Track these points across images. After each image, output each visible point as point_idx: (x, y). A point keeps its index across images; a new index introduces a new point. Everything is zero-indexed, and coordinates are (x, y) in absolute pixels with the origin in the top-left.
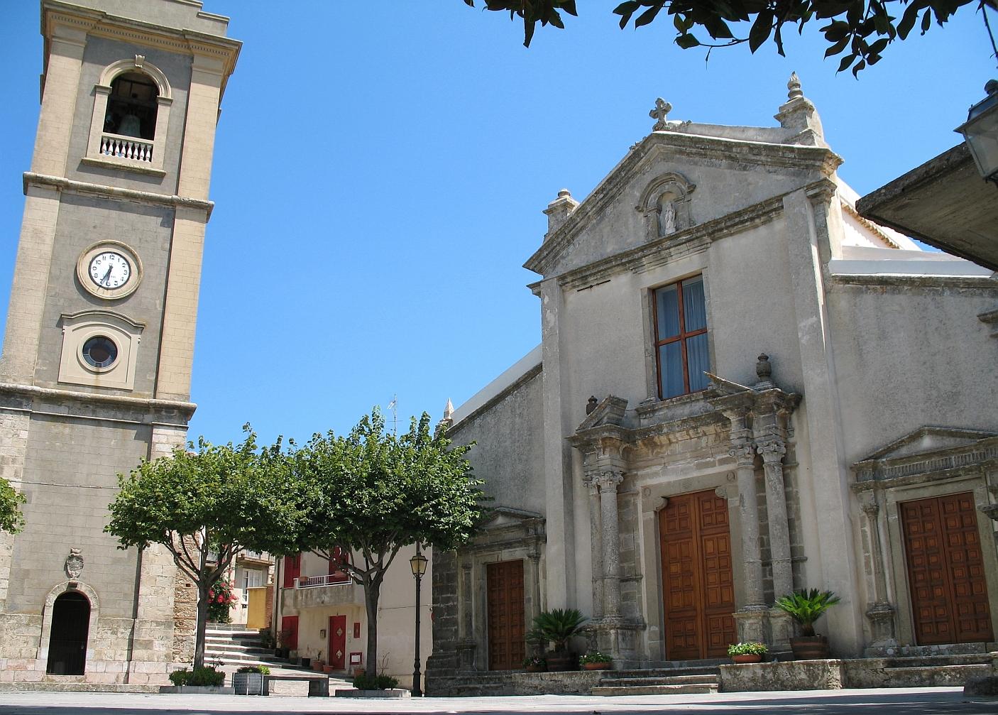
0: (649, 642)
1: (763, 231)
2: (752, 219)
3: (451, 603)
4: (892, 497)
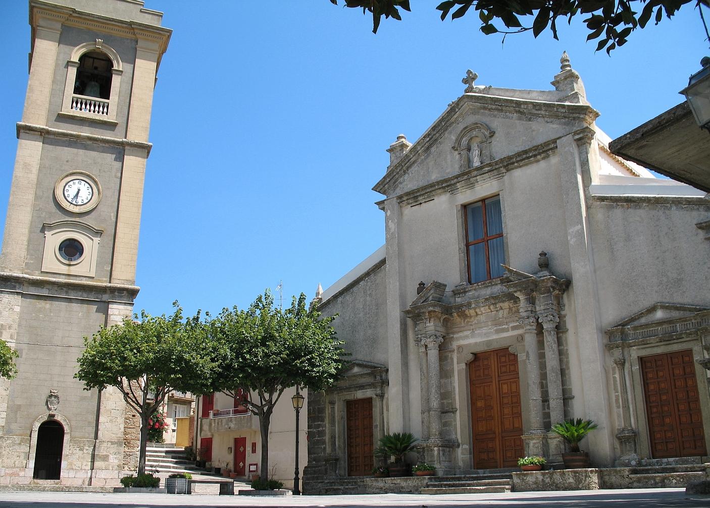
0: (462, 456)
1: (543, 164)
2: (535, 156)
3: (321, 429)
4: (635, 353)
